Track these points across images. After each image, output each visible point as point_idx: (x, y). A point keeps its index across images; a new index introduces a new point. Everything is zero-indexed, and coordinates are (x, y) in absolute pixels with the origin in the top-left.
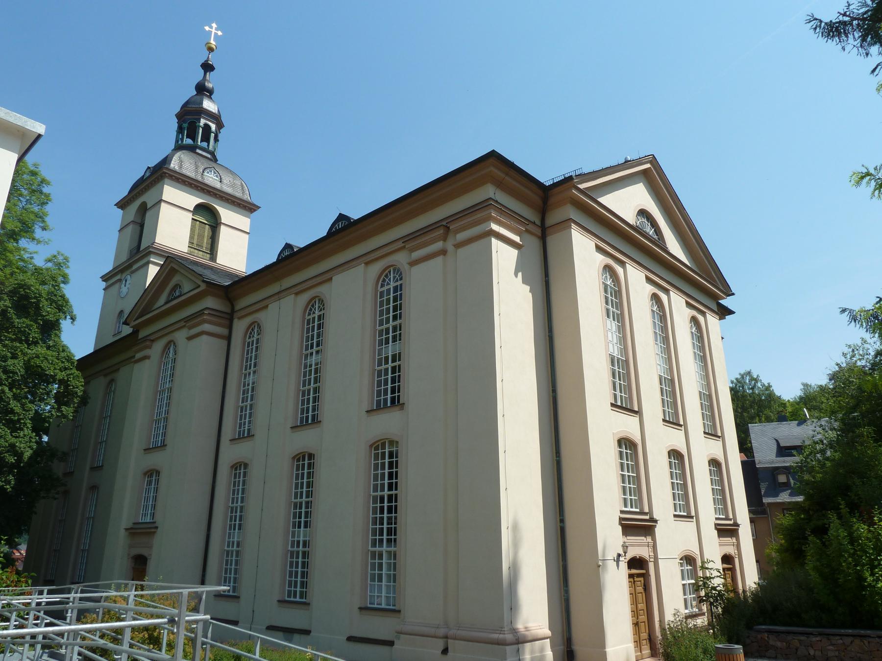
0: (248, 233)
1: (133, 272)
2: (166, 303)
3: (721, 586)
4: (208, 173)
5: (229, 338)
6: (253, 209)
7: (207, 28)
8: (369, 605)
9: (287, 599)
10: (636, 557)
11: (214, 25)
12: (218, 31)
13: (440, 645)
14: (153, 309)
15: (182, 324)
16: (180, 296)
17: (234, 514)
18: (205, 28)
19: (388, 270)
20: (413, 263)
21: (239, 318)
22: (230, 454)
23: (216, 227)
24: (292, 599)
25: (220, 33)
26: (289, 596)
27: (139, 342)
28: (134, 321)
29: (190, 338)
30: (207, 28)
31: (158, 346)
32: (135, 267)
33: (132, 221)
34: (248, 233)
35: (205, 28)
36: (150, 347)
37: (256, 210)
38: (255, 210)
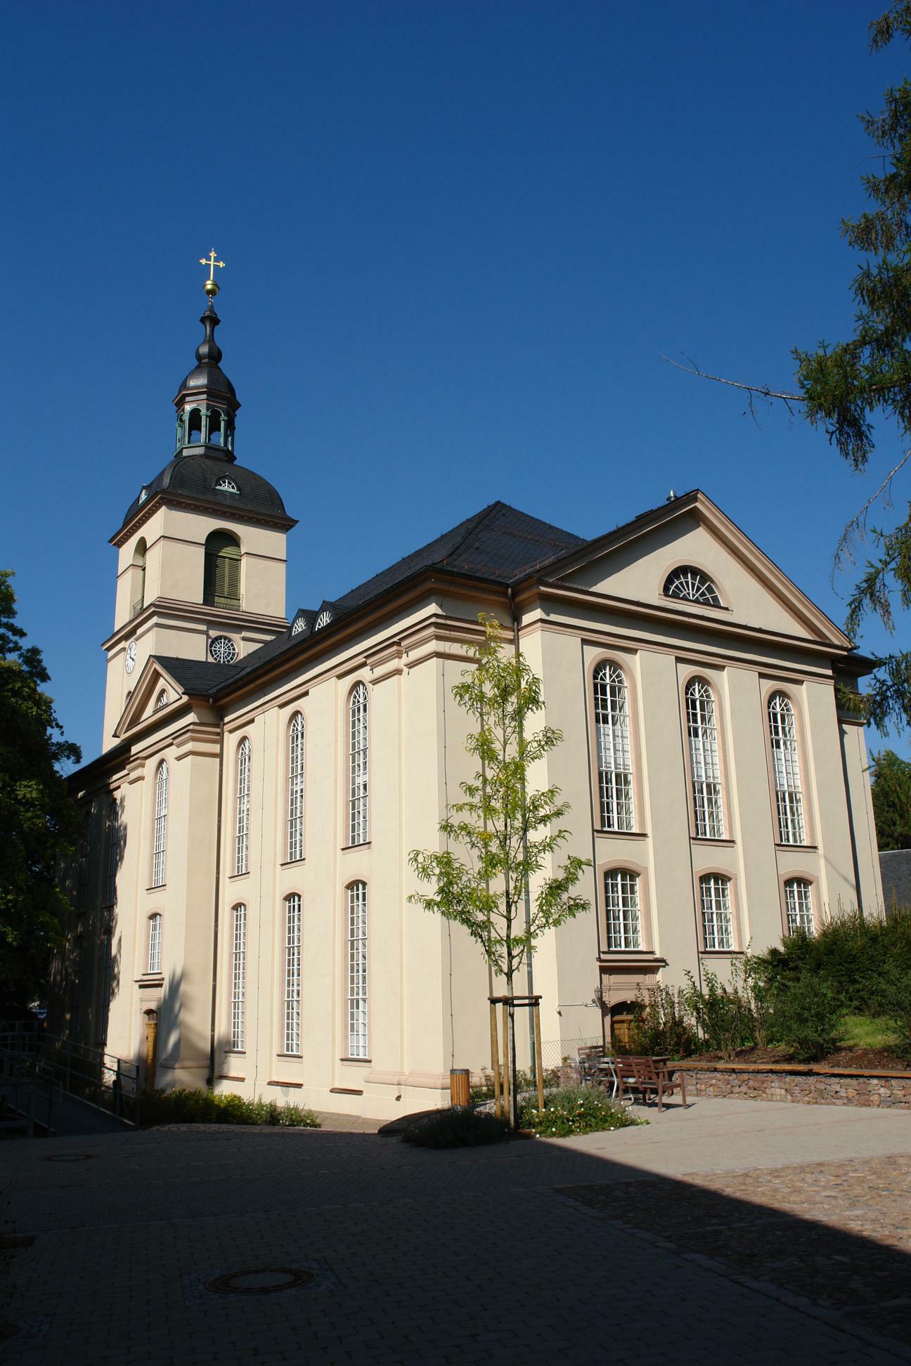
0: (286, 561)
1: (137, 639)
2: (155, 712)
3: (696, 1031)
4: (221, 485)
5: (220, 756)
6: (289, 525)
7: (203, 261)
8: (350, 1056)
9: (286, 1053)
10: (626, 1002)
11: (213, 254)
12: (219, 262)
13: (395, 1091)
14: (141, 721)
15: (169, 741)
16: (167, 705)
17: (291, 957)
18: (201, 261)
19: (352, 697)
20: (375, 682)
21: (231, 731)
22: (230, 894)
23: (240, 560)
24: (290, 1053)
25: (221, 264)
26: (288, 1050)
27: (131, 759)
28: (124, 733)
29: (179, 758)
30: (203, 261)
31: (152, 763)
32: (139, 631)
33: (131, 565)
34: (286, 561)
35: (201, 261)
36: (143, 766)
37: (293, 526)
38: (291, 527)
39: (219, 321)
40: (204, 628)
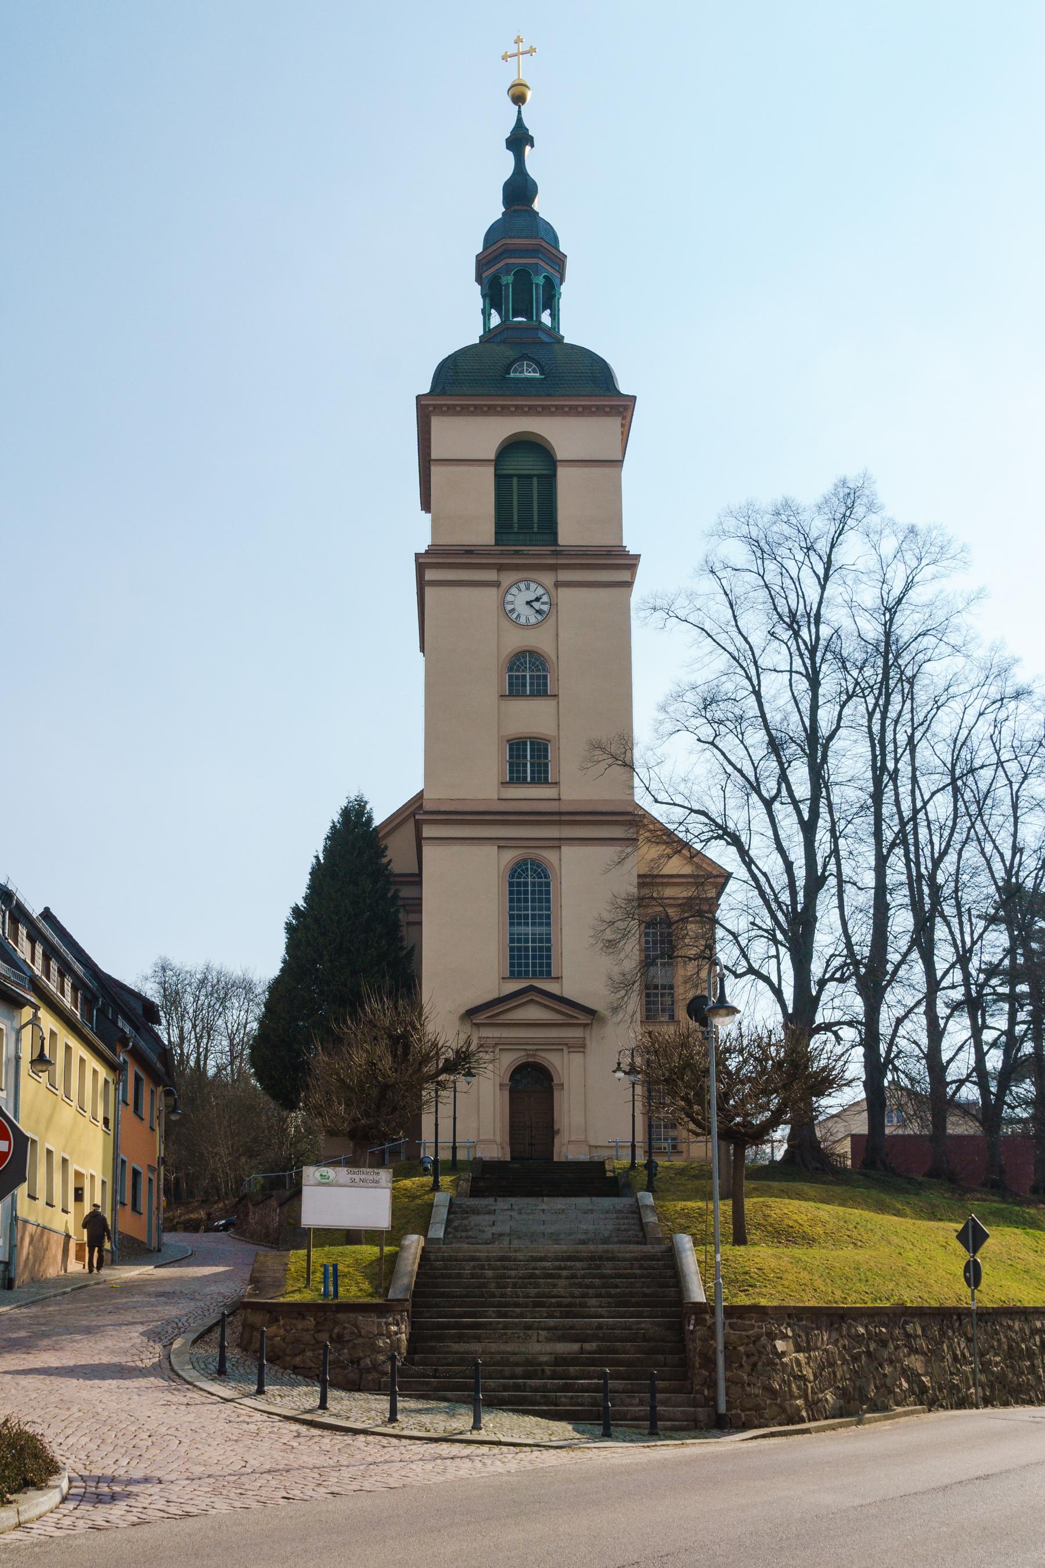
39: (635, 398)
40: (491, 575)
